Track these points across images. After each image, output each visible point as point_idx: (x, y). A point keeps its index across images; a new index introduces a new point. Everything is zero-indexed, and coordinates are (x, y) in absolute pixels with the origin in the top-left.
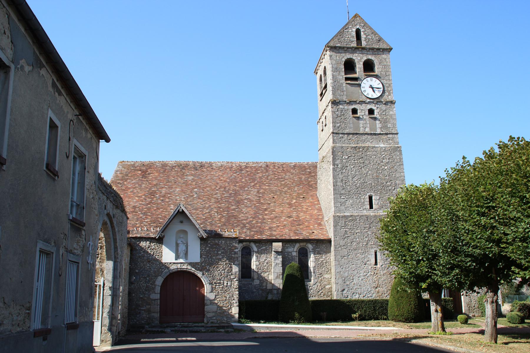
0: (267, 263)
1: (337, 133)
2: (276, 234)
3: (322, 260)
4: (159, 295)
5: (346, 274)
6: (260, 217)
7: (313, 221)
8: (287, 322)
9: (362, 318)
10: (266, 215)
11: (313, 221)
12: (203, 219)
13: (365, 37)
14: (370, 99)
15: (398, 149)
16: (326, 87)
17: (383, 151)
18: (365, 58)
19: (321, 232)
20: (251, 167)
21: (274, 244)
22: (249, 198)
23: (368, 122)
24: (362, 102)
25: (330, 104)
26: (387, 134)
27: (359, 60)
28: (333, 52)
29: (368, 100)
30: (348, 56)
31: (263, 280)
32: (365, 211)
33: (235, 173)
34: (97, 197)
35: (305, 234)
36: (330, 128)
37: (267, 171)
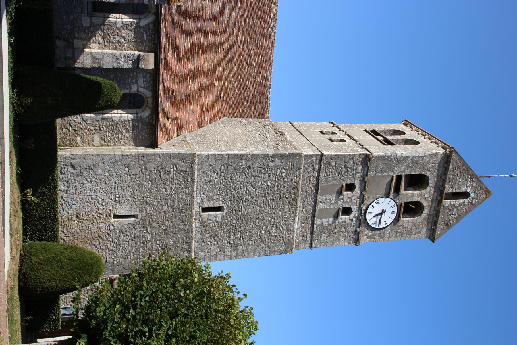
0: (119, 42)
1: (321, 161)
2: (168, 58)
3: (124, 131)
5: (99, 172)
6: (196, 30)
7: (185, 117)
8: (14, 84)
9: (25, 205)
10: (198, 39)
11: (185, 117)
13: (456, 205)
14: (366, 210)
15: (288, 248)
16: (389, 143)
17: (287, 228)
18: (425, 204)
19: (169, 129)
20: (269, 11)
21: (152, 56)
22: (224, 9)
23: (332, 207)
24: (362, 198)
25: (365, 152)
26: (312, 233)
28: (442, 158)
29: (364, 208)
30: (432, 181)
31: (88, 35)
32: (199, 201)
35: (166, 105)
36: (330, 150)
37: (262, 37)
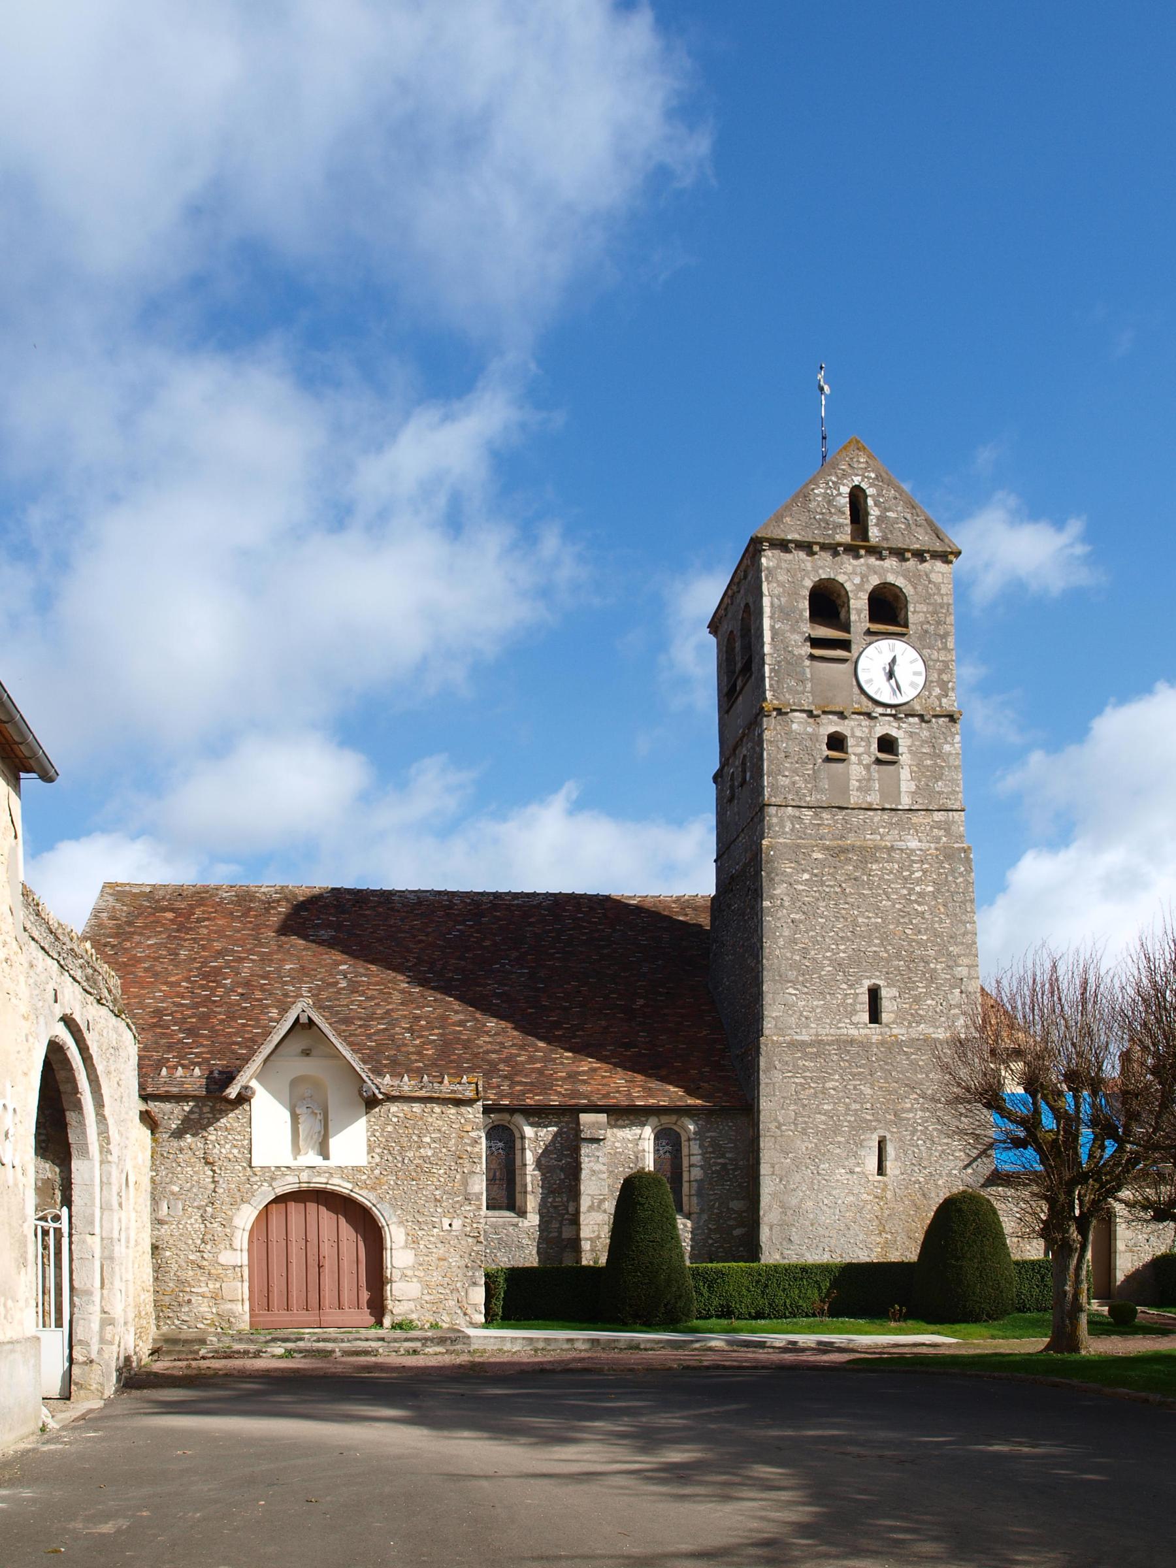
4: (245, 1255)
12: (370, 1048)
33: (463, 923)
34: (23, 959)
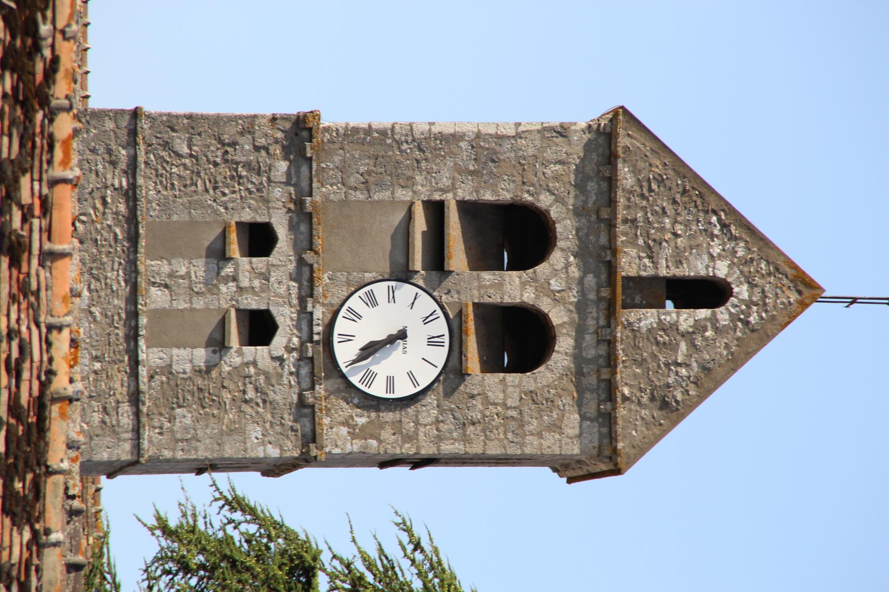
14: (330, 327)
18: (557, 316)
24: (306, 278)
26: (135, 398)
27: (551, 287)
28: (588, 147)
